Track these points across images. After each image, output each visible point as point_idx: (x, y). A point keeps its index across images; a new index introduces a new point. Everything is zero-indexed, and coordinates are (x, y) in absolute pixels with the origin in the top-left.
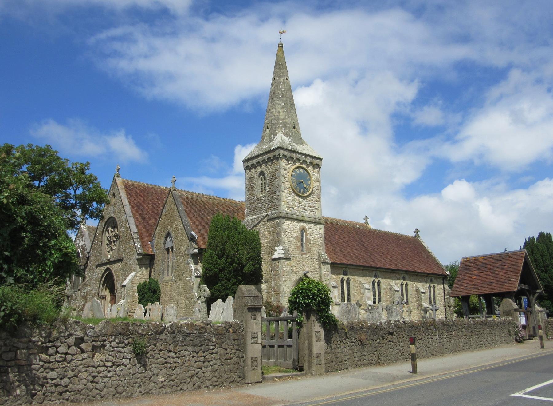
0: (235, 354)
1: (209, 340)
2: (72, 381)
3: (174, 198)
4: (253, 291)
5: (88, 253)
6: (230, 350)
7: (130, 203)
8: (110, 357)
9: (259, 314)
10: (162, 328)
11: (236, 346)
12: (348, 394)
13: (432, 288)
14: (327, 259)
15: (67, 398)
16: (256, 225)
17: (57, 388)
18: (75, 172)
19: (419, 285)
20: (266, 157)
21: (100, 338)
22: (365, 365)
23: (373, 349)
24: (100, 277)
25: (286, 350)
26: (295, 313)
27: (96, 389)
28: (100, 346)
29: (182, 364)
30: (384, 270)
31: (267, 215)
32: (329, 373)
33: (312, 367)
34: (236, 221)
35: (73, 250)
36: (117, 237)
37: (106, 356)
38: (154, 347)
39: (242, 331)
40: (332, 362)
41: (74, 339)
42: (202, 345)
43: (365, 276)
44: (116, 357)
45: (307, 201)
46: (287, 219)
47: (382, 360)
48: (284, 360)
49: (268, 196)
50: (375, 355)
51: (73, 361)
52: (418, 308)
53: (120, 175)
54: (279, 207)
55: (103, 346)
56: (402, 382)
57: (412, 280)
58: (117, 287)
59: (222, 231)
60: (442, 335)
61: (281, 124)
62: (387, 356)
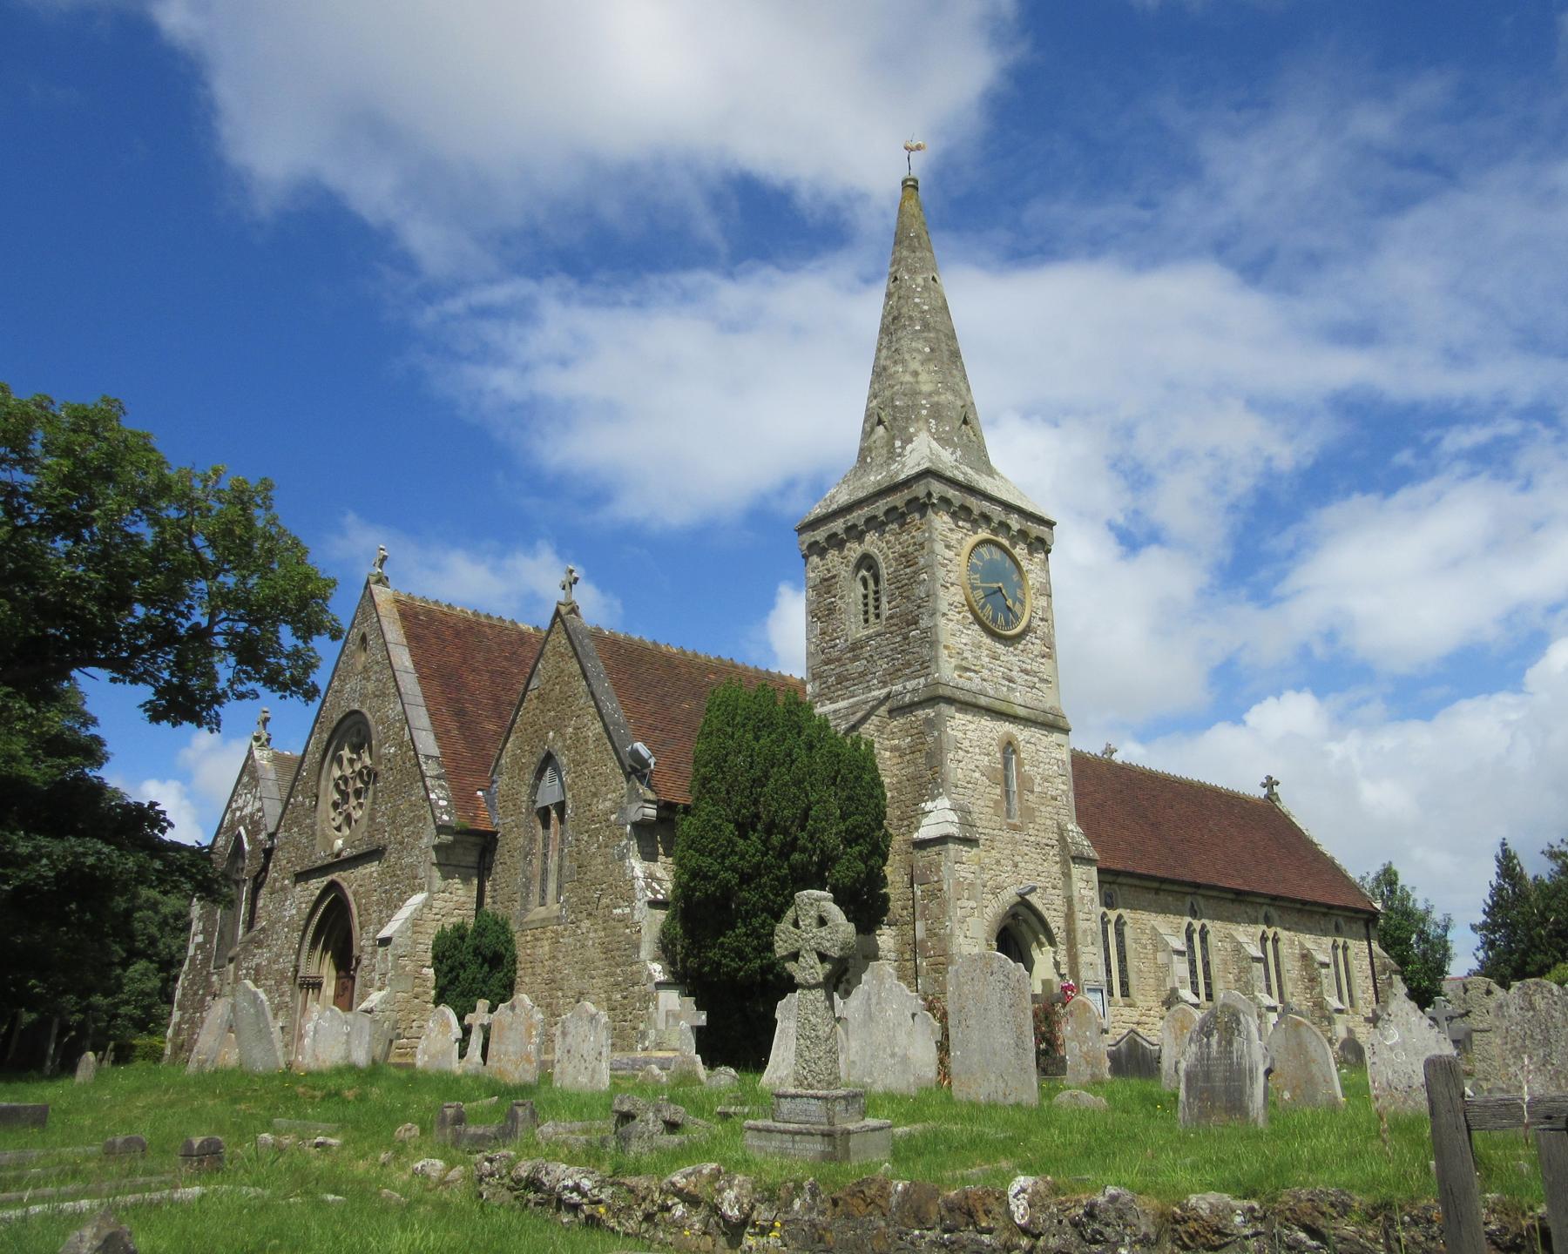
3: (569, 638)
5: (272, 836)
7: (416, 664)
13: (1340, 952)
16: (854, 727)
19: (1309, 941)
20: (882, 506)
31: (888, 697)
36: (370, 776)
43: (1163, 910)
46: (958, 705)
49: (891, 633)
53: (387, 578)
54: (933, 667)
58: (362, 949)
59: (749, 736)
61: (926, 408)
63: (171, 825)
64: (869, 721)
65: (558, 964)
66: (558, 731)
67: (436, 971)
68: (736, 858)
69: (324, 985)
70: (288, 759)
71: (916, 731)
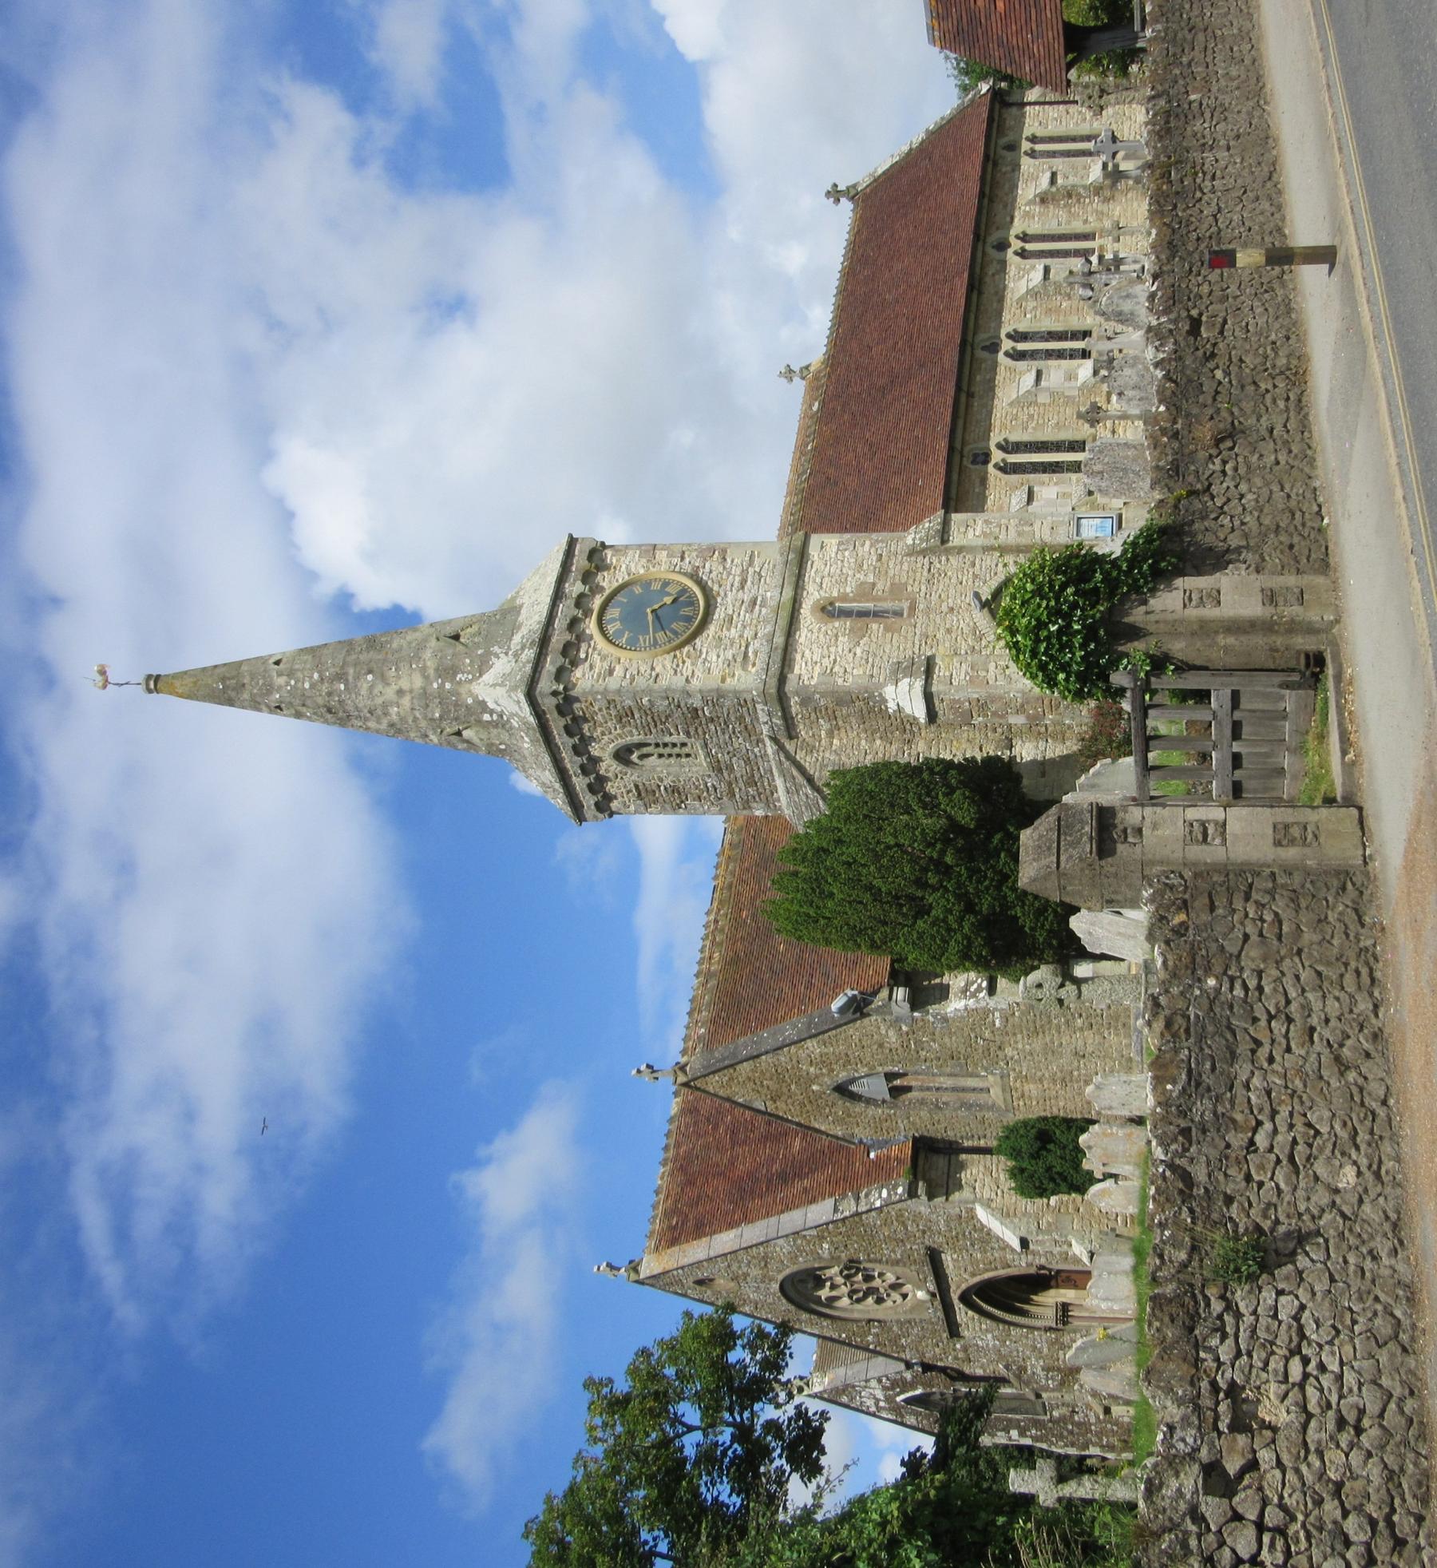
0: (1260, 906)
1: (1212, 1002)
2: (1357, 1502)
3: (714, 1073)
4: (1041, 836)
5: (909, 1365)
6: (1247, 922)
7: (731, 1225)
8: (1272, 1365)
9: (1120, 815)
10: (1168, 1173)
11: (1234, 901)
12: (1407, 507)
13: (1039, 147)
14: (932, 523)
15: (1412, 1520)
16: (810, 780)
17: (1379, 1558)
18: (619, 1429)
19: (1026, 192)
20: (562, 741)
21: (1206, 1402)
22: (1304, 427)
23: (1246, 396)
24: (994, 1324)
25: (1247, 714)
26: (1118, 678)
27: (1381, 1415)
28: (1234, 1402)
29: (1296, 1100)
30: (972, 316)
31: (774, 740)
32: (1331, 560)
33: (1310, 622)
34: (795, 850)
35: (894, 1498)
36: (851, 1267)
37: (1268, 1381)
38: (1235, 1205)
39: (1182, 877)
40: (1291, 547)
41: (1209, 1499)
42: (1229, 1027)
43: (990, 388)
44: (1272, 1343)
45: (722, 594)
47: (1289, 363)
48: (1285, 718)
49: (705, 733)
50: (1270, 387)
51: (1287, 1500)
52: (1107, 200)
53: (631, 1262)
54: (745, 695)
55: (1233, 1390)
56: (1366, 307)
57: (1008, 219)
58: (1029, 1265)
59: (830, 904)
60: (1204, 137)
61: (443, 685)
62: (1274, 343)
63: (918, 1449)
64: (802, 762)
65: (1047, 1075)
66: (813, 1082)
67: (1054, 1193)
68: (950, 917)
69: (1064, 1300)
70: (820, 1357)
71: (813, 714)
